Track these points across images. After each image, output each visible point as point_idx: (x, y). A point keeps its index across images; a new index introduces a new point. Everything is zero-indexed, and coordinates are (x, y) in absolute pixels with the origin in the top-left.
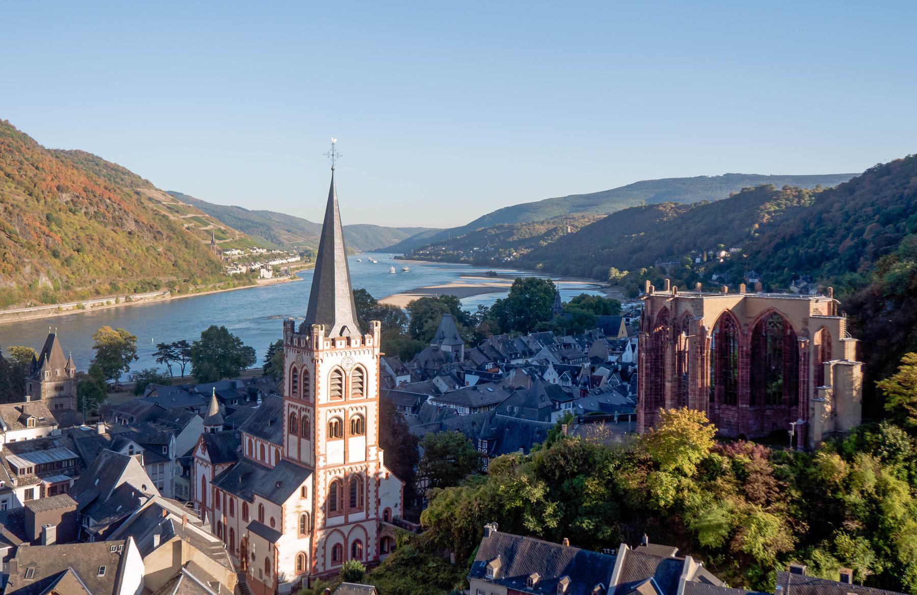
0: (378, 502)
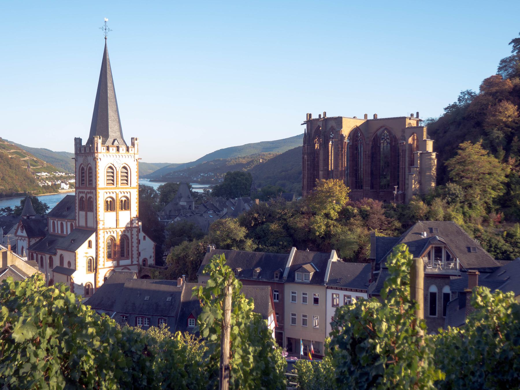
0: (139, 254)
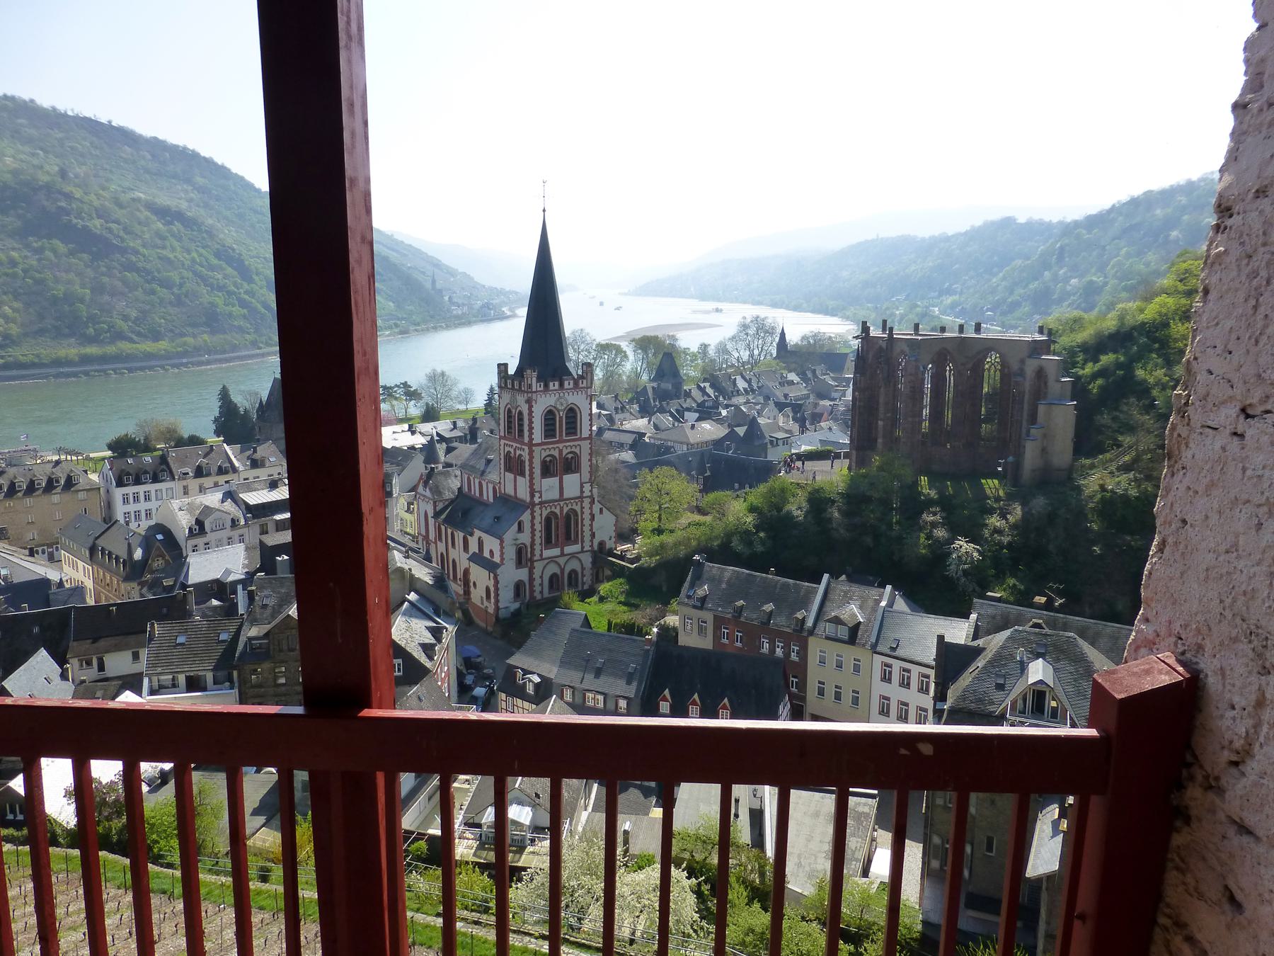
0: (593, 535)
